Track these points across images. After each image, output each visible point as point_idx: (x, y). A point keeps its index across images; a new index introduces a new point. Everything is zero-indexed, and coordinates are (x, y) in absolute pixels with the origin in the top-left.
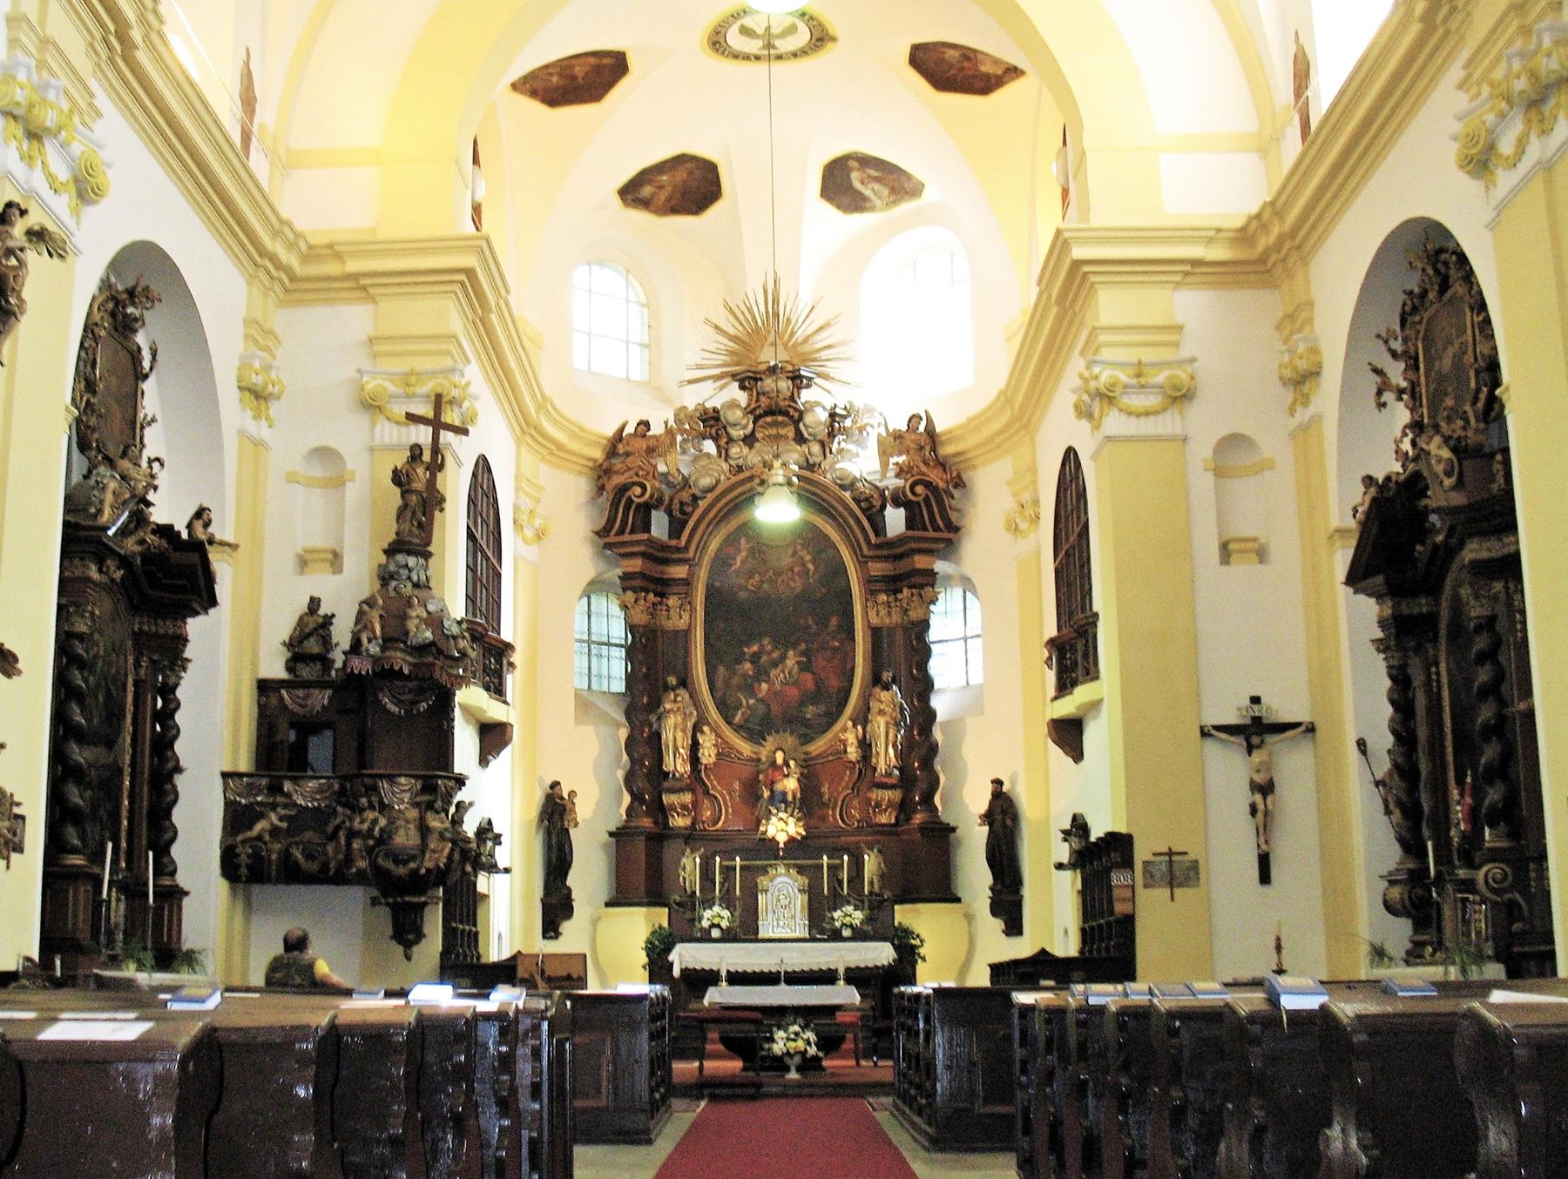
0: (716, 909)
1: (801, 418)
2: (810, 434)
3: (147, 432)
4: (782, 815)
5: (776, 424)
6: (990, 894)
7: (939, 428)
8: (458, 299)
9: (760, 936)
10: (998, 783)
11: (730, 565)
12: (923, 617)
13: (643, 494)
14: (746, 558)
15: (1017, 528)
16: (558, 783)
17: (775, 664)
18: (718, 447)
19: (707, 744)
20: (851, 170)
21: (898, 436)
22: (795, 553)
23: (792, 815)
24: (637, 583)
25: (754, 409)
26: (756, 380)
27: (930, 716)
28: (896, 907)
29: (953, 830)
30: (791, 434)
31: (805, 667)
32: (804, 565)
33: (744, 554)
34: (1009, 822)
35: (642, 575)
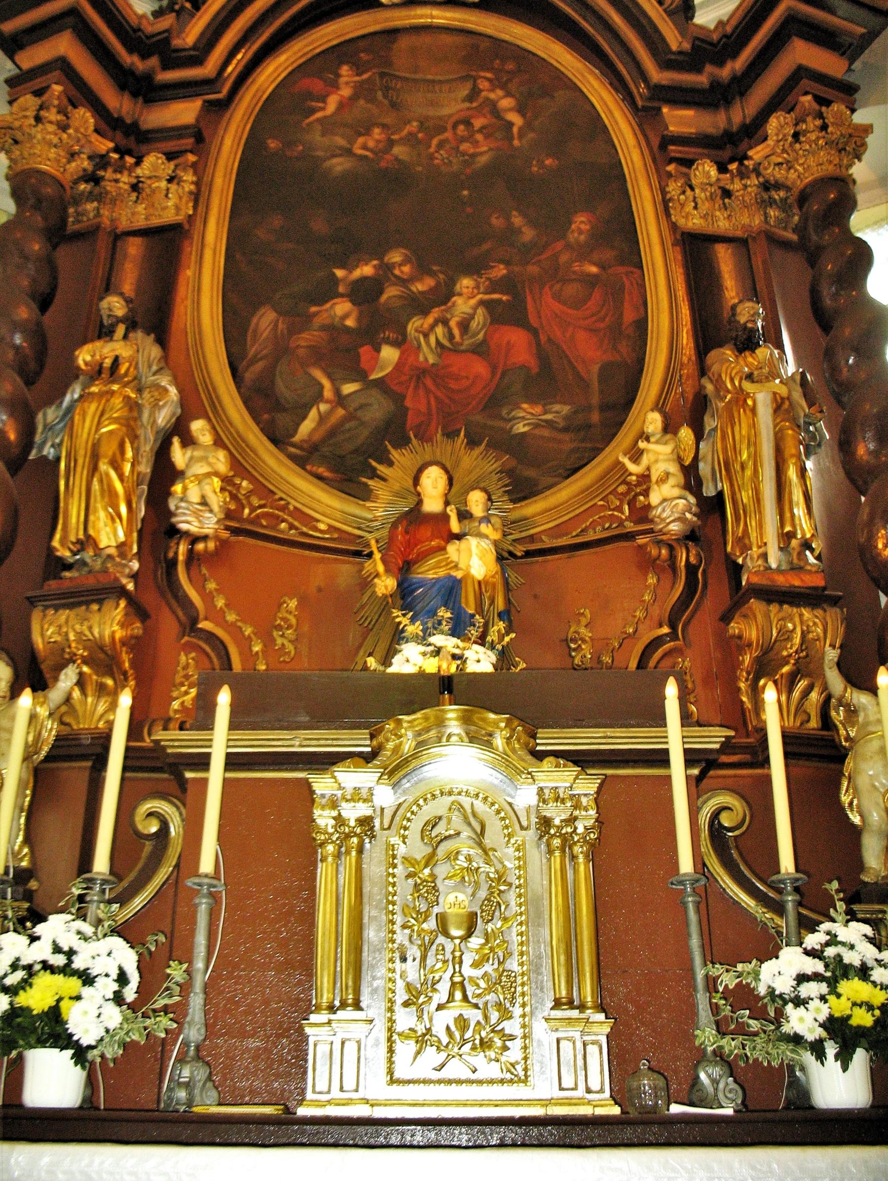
8: (601, 1053)
11: (313, 111)
14: (354, 98)
23: (482, 640)
32: (495, 112)
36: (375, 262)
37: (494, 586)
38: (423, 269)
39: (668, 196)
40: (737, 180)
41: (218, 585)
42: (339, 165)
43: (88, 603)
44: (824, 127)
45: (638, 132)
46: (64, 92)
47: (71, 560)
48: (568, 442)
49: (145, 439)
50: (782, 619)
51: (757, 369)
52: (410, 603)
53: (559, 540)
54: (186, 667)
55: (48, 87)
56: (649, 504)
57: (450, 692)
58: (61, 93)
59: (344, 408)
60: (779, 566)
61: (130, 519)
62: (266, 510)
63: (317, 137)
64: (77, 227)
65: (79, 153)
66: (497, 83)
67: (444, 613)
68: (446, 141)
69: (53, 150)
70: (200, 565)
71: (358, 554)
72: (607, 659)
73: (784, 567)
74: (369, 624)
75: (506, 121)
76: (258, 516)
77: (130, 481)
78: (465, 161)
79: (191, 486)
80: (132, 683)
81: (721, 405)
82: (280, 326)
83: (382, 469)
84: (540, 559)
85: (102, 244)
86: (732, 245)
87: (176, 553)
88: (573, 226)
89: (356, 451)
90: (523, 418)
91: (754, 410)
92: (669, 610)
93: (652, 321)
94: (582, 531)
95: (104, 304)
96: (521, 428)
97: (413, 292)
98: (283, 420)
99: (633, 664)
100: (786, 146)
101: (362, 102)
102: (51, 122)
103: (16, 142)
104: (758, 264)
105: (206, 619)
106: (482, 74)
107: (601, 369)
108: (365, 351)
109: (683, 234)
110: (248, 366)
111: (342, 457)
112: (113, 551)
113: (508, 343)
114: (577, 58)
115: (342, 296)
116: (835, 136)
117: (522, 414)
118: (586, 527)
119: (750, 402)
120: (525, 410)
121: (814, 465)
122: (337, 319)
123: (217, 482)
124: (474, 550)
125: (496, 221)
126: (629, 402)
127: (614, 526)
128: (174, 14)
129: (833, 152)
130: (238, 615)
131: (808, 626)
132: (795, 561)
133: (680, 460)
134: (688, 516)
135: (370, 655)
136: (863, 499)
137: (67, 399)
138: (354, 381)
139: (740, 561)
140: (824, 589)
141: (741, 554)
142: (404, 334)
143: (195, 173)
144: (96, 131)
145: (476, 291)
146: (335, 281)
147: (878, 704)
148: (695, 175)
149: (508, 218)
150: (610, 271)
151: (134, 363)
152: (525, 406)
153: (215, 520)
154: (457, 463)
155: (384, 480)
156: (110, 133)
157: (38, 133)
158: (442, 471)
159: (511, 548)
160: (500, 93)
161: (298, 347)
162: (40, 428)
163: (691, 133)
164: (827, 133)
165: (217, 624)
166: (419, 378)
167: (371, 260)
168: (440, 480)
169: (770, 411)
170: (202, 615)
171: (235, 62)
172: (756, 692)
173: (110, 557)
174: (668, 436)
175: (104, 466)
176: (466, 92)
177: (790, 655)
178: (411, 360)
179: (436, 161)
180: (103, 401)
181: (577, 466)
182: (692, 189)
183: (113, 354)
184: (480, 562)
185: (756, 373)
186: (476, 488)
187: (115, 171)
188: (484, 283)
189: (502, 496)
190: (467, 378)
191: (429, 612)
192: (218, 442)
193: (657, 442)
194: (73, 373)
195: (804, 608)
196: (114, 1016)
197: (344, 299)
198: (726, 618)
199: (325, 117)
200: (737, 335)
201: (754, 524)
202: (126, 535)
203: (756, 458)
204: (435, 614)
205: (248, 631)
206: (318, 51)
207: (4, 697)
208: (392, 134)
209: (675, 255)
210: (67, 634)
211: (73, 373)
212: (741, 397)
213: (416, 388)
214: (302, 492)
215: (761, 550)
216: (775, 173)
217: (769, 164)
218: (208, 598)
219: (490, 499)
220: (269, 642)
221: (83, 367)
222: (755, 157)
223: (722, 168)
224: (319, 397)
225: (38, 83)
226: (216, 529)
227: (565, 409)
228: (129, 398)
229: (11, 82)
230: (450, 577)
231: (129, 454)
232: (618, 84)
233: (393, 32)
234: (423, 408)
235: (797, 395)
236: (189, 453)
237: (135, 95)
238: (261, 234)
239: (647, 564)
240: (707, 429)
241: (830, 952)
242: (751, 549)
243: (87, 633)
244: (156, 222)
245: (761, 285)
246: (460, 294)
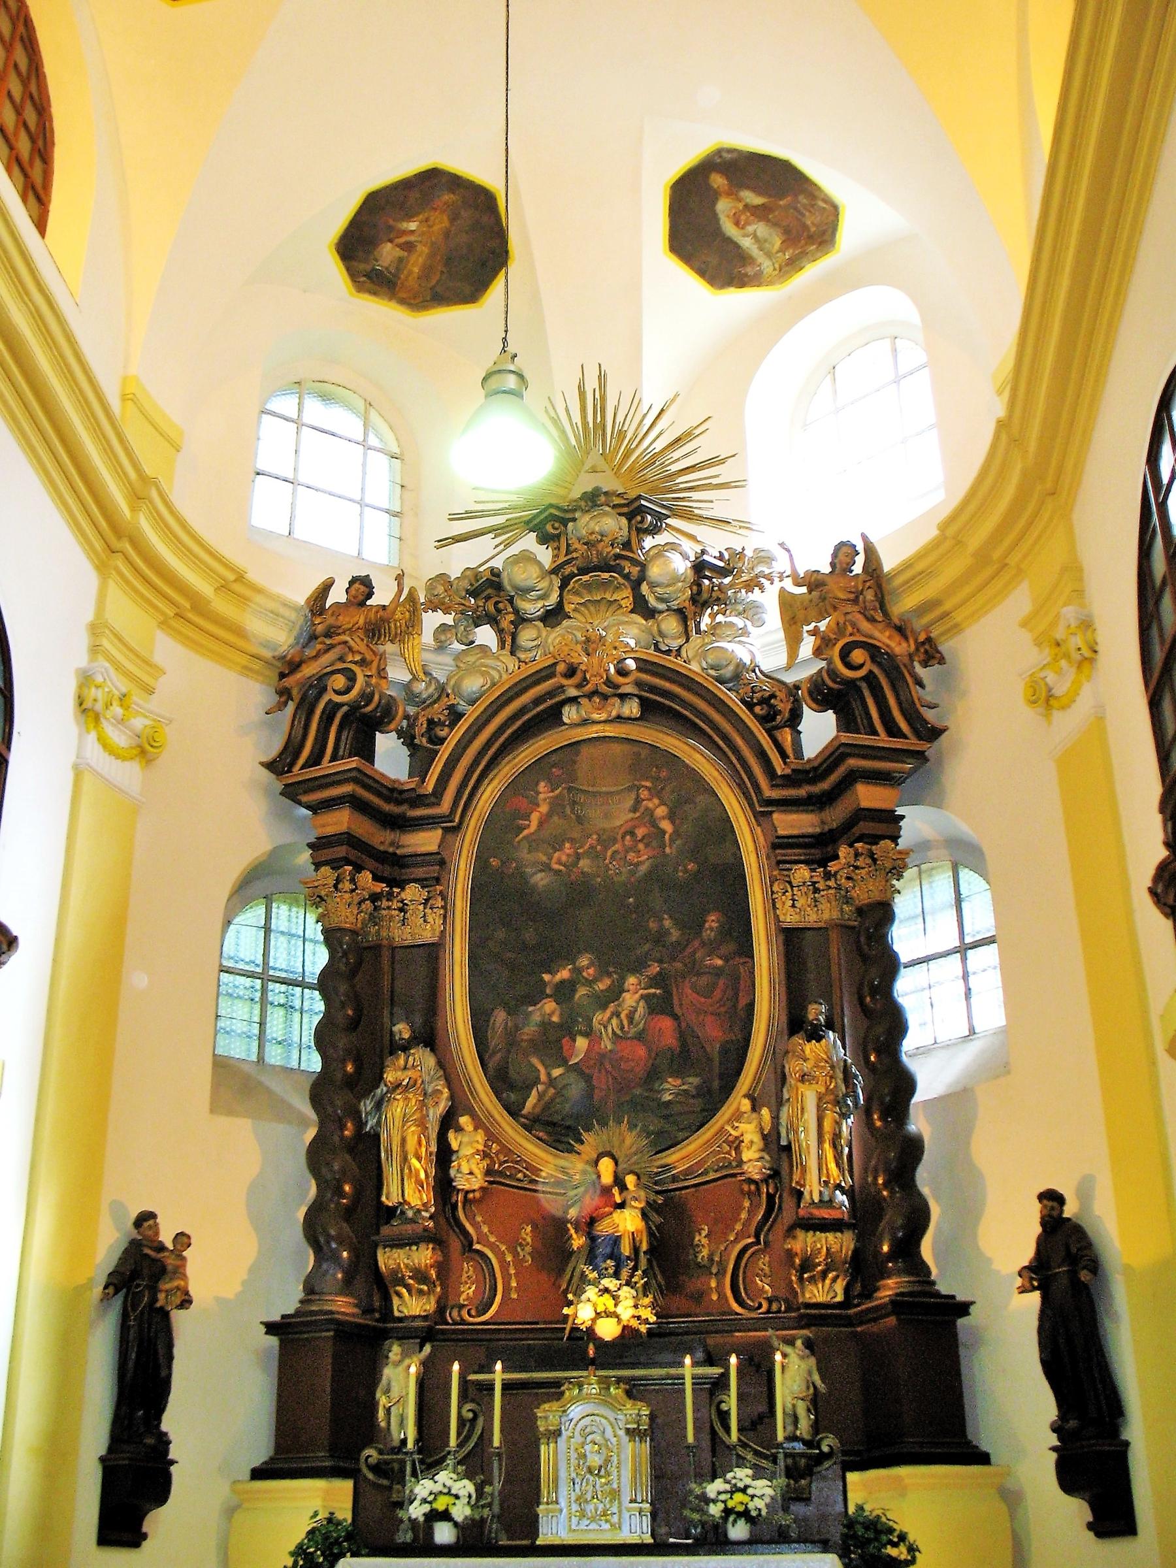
0: (444, 1477)
1: (642, 578)
2: (661, 600)
4: (610, 1283)
5: (605, 585)
6: (1053, 1440)
7: (889, 564)
9: (548, 1534)
10: (1052, 1198)
11: (521, 829)
12: (876, 896)
13: (348, 690)
14: (549, 815)
15: (1050, 696)
16: (151, 1216)
18: (500, 632)
19: (467, 1151)
20: (715, 196)
21: (814, 582)
22: (638, 801)
23: (628, 1284)
24: (341, 851)
25: (561, 566)
26: (564, 522)
27: (905, 1084)
28: (852, 1477)
29: (964, 1309)
30: (628, 603)
31: (660, 1005)
32: (653, 823)
33: (544, 808)
34: (1084, 1276)
35: (349, 839)
36: (570, 967)
48: (698, 1104)
59: (555, 1088)
63: (524, 854)
66: (656, 793)
75: (658, 828)
83: (577, 1146)
88: (707, 925)
95: (396, 1029)
96: (667, 1097)
101: (555, 818)
110: (490, 1057)
115: (548, 996)
125: (653, 925)
133: (762, 1129)
138: (559, 1066)
142: (591, 1027)
146: (544, 984)
152: (670, 1080)
170: (475, 1238)
179: (610, 872)
196: (468, 1511)
209: (781, 938)
220: (515, 1255)
224: (537, 1081)
227: (695, 1081)
231: (424, 1142)
241: (734, 1481)
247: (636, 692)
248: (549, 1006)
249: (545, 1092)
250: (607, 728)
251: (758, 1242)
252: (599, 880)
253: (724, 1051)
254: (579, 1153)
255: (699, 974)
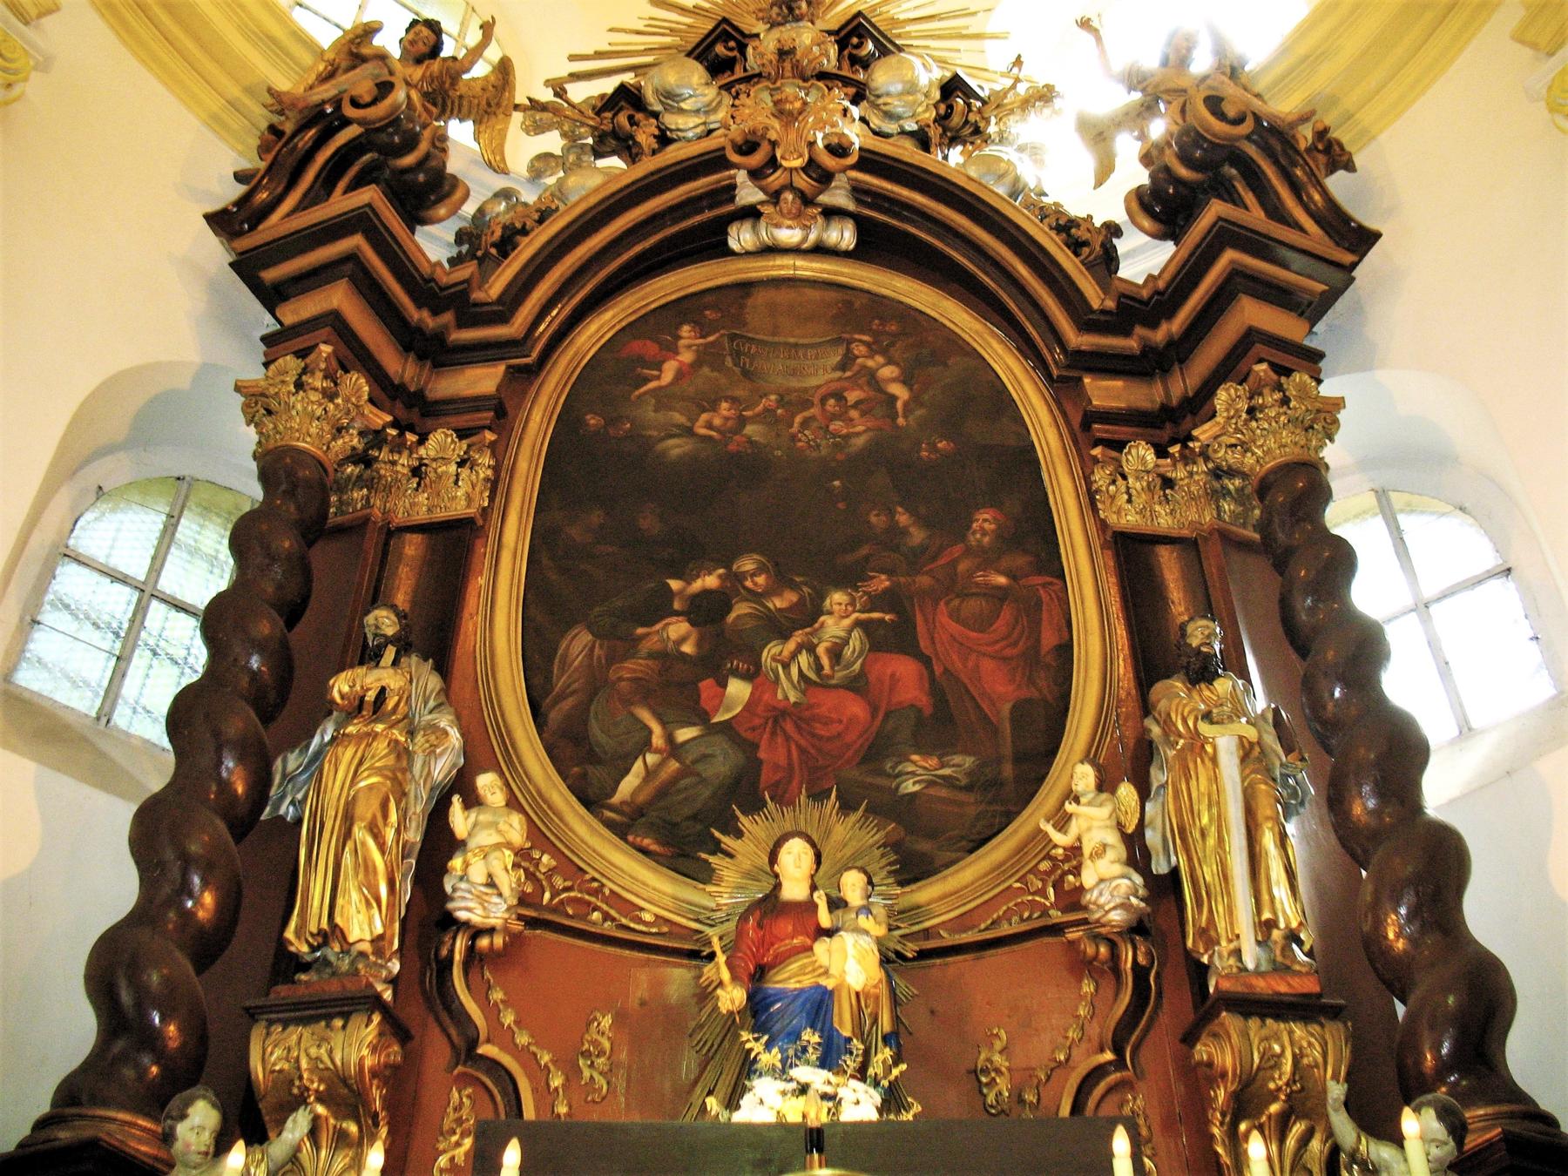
3: (836, 27)
11: (647, 380)
14: (697, 364)
17: (779, 627)
23: (861, 1074)
31: (880, 639)
32: (871, 377)
33: (687, 357)
36: (721, 571)
37: (877, 998)
38: (782, 580)
39: (1094, 487)
40: (1180, 466)
41: (505, 994)
42: (676, 448)
43: (329, 1018)
44: (1285, 401)
45: (1054, 408)
46: (335, 352)
47: (309, 958)
48: (972, 806)
49: (416, 797)
50: (1267, 1039)
51: (1216, 706)
52: (764, 1023)
53: (964, 935)
54: (457, 1109)
55: (317, 345)
56: (1081, 885)
57: (820, 1151)
58: (329, 354)
59: (678, 759)
60: (1257, 966)
61: (390, 905)
62: (572, 894)
63: (649, 413)
64: (339, 519)
65: (347, 429)
67: (811, 1037)
68: (813, 418)
69: (315, 424)
70: (482, 968)
71: (694, 955)
72: (1030, 1097)
73: (1264, 967)
74: (709, 1050)
75: (886, 393)
76: (562, 902)
77: (394, 851)
78: (835, 445)
79: (473, 860)
80: (384, 1132)
81: (1171, 753)
82: (597, 651)
83: (728, 841)
84: (938, 961)
85: (372, 541)
86: (1178, 546)
87: (452, 951)
88: (974, 525)
89: (694, 817)
90: (913, 774)
91: (1214, 760)
92: (1112, 1028)
93: (1079, 645)
94: (992, 923)
95: (370, 619)
96: (910, 787)
97: (769, 609)
98: (596, 773)
99: (1065, 1111)
100: (1240, 423)
101: (706, 370)
102: (316, 389)
103: (269, 412)
104: (1211, 567)
105: (488, 1041)
106: (857, 336)
107: (1014, 706)
108: (707, 686)
109: (1115, 533)
110: (553, 706)
111: (675, 825)
112: (366, 947)
113: (893, 675)
114: (976, 319)
115: (677, 613)
116: (1299, 412)
117: (911, 768)
118: (999, 917)
119: (1209, 749)
120: (914, 763)
121: (1298, 829)
122: (670, 645)
123: (509, 857)
124: (851, 951)
125: (877, 520)
126: (1052, 752)
127: (1036, 915)
128: (476, 262)
129: (1298, 431)
130: (532, 1036)
131: (1301, 1048)
132: (1279, 959)
133: (1120, 827)
134: (1134, 901)
135: (710, 1093)
136: (1364, 873)
137: (316, 741)
138: (694, 724)
139: (1205, 959)
140: (1319, 996)
141: (1206, 951)
143: (493, 455)
144: (371, 400)
145: (850, 608)
147: (1406, 1160)
148: (1127, 460)
149: (891, 513)
150: (1023, 582)
151: (405, 696)
152: (915, 757)
153: (505, 907)
154: (828, 833)
155: (730, 855)
156: (387, 402)
157: (298, 401)
158: (808, 846)
159: (899, 948)
160: (880, 359)
161: (620, 679)
162: (277, 779)
163: (1121, 409)
164: (1289, 408)
165: (502, 1048)
166: (776, 721)
167: (715, 569)
168: (803, 856)
169: (1236, 761)
170: (483, 1035)
171: (548, 319)
172: (1236, 1142)
173: (362, 954)
174: (1104, 796)
175: (360, 833)
176: (839, 358)
177: (1279, 1089)
178: (766, 697)
179: (800, 444)
180: (363, 746)
181: (982, 836)
182: (1124, 477)
183: (378, 685)
184: (859, 968)
185: (1215, 711)
186: (850, 868)
187: (391, 451)
188: (861, 597)
189: (887, 877)
190: (840, 721)
191: (789, 1034)
192: (513, 803)
193: (1090, 804)
194: (327, 708)
195: (1294, 1021)
197: (680, 618)
198: (1190, 1038)
199: (660, 388)
200: (1189, 663)
201: (1221, 909)
202: (384, 926)
203: (1220, 821)
204: (799, 1037)
205: (545, 1058)
206: (653, 306)
207: (207, 1154)
208: (744, 410)
209: (1106, 560)
210: (297, 1060)
211: (327, 708)
212: (1198, 744)
213: (773, 733)
214: (622, 870)
215: (1232, 946)
216: (1228, 457)
217: (1220, 445)
218: (491, 1011)
219: (870, 882)
220: (572, 1073)
221: (338, 700)
222: (1201, 437)
223: (1161, 452)
224: (646, 745)
225: (300, 343)
226: (506, 920)
227: (968, 761)
228: (397, 741)
229: (268, 340)
230: (819, 986)
231: (393, 817)
232: (1027, 348)
233: (746, 287)
234: (783, 761)
235: (1271, 739)
236: (473, 815)
237: (421, 357)
238: (575, 533)
239: (1081, 966)
240: (1155, 786)
242: (1218, 943)
243: (326, 1058)
244: (440, 515)
245: (1216, 596)
246: (830, 613)
247: (851, 206)
248: (677, 628)
249: (660, 765)
250: (799, 263)
251: (1119, 1063)
252: (780, 453)
253: (1021, 712)
254: (730, 855)
255: (964, 596)
